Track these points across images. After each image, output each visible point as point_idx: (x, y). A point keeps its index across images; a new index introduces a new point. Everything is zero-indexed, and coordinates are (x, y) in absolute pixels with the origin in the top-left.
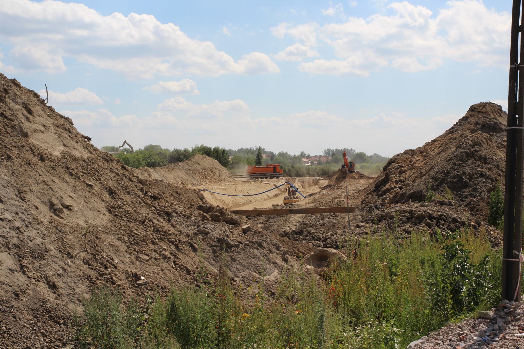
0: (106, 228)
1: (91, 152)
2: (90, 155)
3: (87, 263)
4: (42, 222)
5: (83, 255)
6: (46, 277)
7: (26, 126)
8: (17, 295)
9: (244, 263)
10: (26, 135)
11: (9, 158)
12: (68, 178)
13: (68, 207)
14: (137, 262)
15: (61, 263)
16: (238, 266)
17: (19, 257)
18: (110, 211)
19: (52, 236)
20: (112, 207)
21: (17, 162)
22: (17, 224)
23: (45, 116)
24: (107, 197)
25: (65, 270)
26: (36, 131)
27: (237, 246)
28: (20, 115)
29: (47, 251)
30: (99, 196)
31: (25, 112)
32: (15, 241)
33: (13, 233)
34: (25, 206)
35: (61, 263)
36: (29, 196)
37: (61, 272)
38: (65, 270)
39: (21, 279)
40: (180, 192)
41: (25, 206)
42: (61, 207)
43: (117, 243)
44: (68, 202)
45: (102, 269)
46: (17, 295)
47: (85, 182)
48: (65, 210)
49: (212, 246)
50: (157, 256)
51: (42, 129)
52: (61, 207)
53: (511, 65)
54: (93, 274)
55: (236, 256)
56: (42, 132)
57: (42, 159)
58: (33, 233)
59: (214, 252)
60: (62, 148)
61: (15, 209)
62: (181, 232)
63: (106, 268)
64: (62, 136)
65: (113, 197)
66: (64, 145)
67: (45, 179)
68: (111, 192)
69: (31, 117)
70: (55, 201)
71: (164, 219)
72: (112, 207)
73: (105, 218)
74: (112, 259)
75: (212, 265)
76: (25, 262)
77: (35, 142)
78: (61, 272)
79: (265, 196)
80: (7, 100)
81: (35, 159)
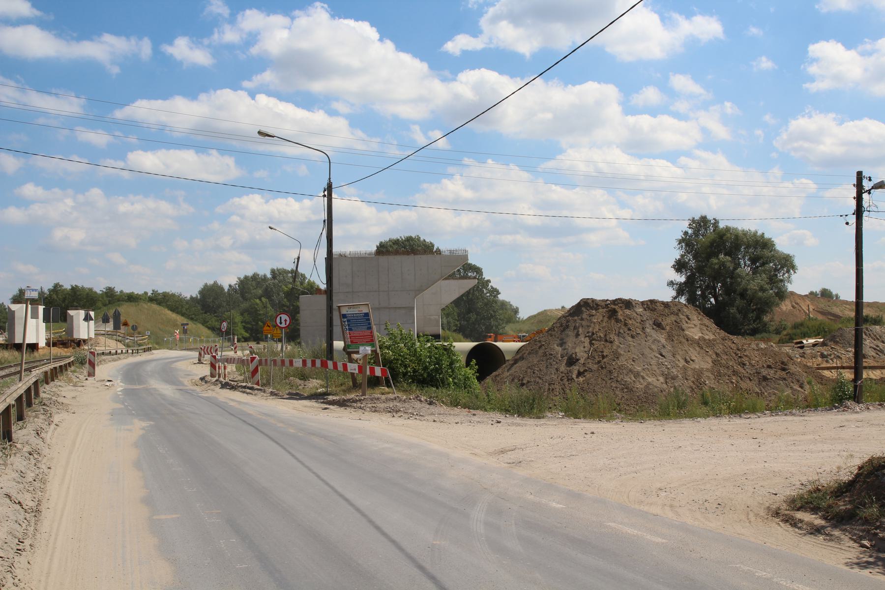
0: (707, 369)
1: (715, 336)
2: (714, 337)
3: (693, 382)
4: (679, 366)
5: (693, 379)
6: (675, 386)
7: (685, 326)
8: (662, 391)
9: (772, 386)
10: (683, 330)
11: (673, 340)
12: (697, 348)
13: (693, 360)
14: (717, 383)
15: (682, 382)
16: (769, 388)
17: (666, 378)
18: (713, 363)
19: (682, 372)
20: (715, 361)
21: (676, 342)
22: (669, 367)
23: (697, 320)
24: (714, 356)
25: (683, 384)
26: (689, 328)
27: (771, 379)
28: (683, 321)
29: (678, 377)
30: (710, 356)
31: (687, 320)
32: (666, 373)
33: (666, 370)
34: (674, 360)
35: (682, 382)
36: (677, 356)
37: (681, 384)
38: (683, 384)
39: (665, 386)
40: (777, 354)
41: (674, 360)
42: (689, 360)
43: (710, 375)
44: (694, 358)
45: (699, 385)
46: (662, 391)
47: (705, 350)
48: (691, 362)
49: (759, 379)
50: (728, 381)
51: (693, 326)
52: (689, 360)
53: (862, 269)
54: (694, 386)
55: (769, 383)
56: (693, 328)
57: (688, 340)
58: (674, 370)
59: (759, 381)
60: (701, 335)
61: (669, 361)
62: (747, 372)
63: (701, 384)
64: (702, 329)
65: (717, 357)
66: (702, 333)
67: (686, 349)
68: (717, 355)
69: (689, 321)
70: (687, 358)
71: (741, 366)
72: (715, 361)
73: (709, 365)
74: (705, 382)
75: (757, 387)
76: (668, 380)
77: (687, 332)
78: (681, 384)
79: (42, 363)
80: (680, 314)
81: (684, 340)
